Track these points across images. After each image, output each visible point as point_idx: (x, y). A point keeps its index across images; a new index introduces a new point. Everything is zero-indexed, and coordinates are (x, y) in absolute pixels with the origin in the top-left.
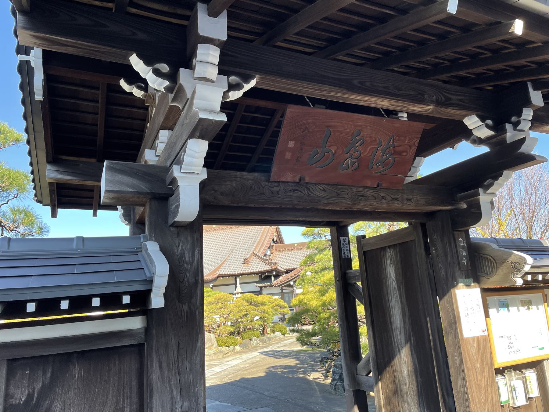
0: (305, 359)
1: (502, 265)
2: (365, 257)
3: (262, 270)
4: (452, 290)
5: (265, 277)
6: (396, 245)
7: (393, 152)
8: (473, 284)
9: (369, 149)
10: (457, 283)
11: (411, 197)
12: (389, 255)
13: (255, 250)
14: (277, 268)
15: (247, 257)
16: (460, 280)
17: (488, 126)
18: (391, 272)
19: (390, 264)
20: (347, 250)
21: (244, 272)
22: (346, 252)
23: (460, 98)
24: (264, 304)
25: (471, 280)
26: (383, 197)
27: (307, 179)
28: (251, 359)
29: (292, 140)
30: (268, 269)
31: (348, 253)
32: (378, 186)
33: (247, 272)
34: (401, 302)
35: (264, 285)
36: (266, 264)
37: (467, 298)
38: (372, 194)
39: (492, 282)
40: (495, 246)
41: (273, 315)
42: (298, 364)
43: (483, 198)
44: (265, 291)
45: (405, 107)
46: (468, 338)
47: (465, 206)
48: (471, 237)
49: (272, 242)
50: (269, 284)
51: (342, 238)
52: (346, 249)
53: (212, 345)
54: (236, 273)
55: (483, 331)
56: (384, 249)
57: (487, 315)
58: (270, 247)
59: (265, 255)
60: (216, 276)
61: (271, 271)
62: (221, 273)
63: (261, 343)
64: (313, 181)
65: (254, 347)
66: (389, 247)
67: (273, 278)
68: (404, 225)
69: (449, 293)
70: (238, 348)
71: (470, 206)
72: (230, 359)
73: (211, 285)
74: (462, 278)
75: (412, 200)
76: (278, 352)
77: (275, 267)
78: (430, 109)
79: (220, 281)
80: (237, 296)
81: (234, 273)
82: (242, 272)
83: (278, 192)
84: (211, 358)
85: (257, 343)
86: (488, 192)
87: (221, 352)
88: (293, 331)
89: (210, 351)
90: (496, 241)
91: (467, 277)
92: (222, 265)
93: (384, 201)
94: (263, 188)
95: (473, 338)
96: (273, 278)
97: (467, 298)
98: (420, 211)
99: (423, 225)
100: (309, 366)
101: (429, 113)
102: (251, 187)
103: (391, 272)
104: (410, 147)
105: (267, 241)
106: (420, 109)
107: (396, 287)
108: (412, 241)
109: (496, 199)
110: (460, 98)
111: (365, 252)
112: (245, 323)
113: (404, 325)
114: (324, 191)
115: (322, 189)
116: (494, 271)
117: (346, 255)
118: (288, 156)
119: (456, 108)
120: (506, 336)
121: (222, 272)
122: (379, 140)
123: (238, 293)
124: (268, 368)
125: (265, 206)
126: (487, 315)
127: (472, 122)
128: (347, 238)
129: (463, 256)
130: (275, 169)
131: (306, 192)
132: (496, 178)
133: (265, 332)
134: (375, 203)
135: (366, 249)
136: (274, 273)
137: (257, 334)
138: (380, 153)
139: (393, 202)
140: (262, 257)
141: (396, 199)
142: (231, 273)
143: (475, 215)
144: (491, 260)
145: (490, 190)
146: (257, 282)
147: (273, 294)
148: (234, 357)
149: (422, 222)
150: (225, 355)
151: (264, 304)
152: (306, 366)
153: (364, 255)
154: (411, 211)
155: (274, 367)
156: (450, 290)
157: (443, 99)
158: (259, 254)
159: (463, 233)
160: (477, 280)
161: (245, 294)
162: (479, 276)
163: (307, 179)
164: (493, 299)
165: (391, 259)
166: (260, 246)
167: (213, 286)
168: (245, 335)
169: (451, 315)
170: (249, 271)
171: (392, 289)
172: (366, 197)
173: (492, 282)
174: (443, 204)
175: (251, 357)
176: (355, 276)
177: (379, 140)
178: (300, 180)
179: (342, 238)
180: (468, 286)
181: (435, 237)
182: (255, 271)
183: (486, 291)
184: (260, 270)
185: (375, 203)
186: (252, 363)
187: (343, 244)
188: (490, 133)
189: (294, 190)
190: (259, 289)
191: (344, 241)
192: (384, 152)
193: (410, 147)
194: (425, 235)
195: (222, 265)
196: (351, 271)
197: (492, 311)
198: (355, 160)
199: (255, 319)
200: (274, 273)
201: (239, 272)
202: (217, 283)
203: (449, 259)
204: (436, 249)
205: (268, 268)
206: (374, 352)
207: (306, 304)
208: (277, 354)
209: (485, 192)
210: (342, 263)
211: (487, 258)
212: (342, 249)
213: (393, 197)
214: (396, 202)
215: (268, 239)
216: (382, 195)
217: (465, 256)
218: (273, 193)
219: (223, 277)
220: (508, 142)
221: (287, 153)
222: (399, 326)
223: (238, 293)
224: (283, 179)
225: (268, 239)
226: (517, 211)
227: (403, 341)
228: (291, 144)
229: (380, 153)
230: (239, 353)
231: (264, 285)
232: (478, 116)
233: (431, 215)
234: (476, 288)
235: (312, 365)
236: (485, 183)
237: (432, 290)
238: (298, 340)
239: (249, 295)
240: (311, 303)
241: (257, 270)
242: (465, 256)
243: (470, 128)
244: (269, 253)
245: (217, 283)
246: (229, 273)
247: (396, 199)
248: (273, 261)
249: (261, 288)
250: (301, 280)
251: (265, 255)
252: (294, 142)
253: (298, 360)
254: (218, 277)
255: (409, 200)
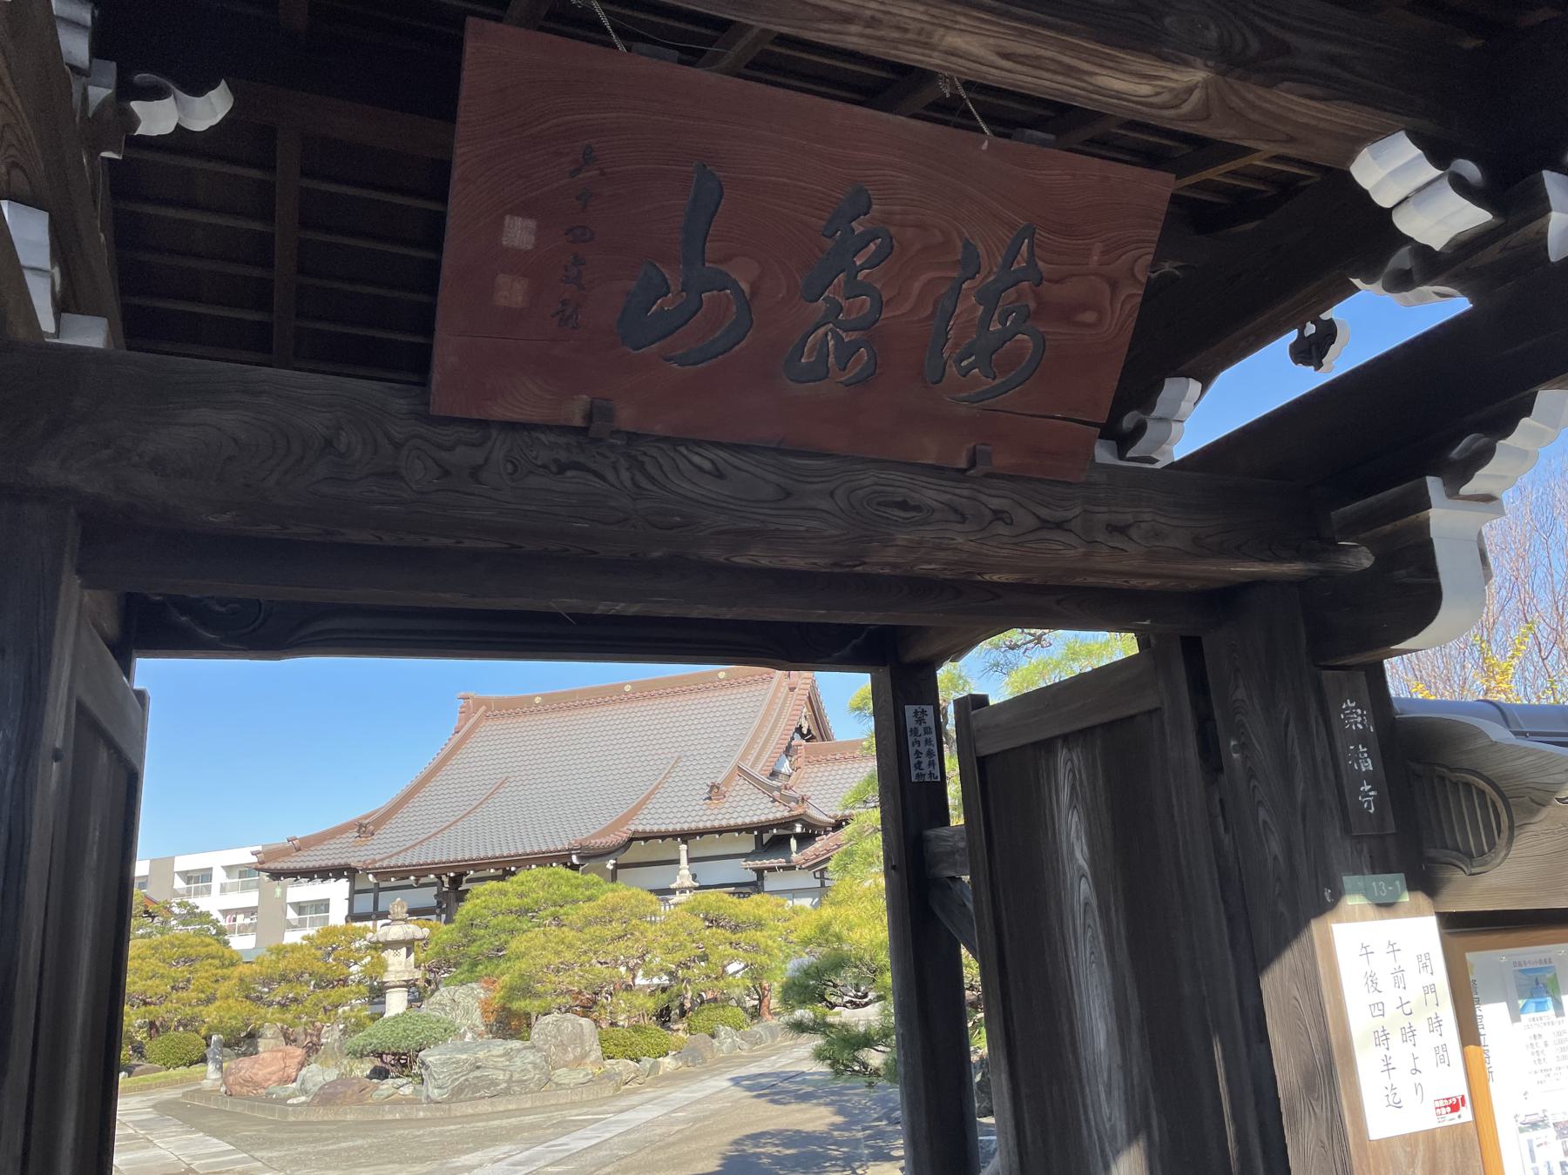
0: (862, 1111)
1: (1533, 813)
2: (984, 783)
3: (763, 818)
4: (1315, 926)
5: (772, 839)
6: (1091, 729)
7: (1032, 305)
8: (1406, 898)
9: (917, 286)
10: (1338, 895)
11: (1130, 518)
12: (1067, 777)
13: (743, 757)
14: (805, 814)
15: (719, 781)
16: (1348, 881)
17: (1461, 186)
18: (1074, 842)
19: (1072, 806)
20: (930, 753)
21: (709, 825)
22: (925, 760)
23: (1334, 49)
24: (759, 925)
25: (1398, 880)
26: (998, 515)
27: (626, 417)
28: (698, 1101)
29: (523, 210)
30: (779, 815)
31: (931, 764)
32: (973, 463)
33: (716, 824)
34: (1113, 964)
35: (766, 863)
36: (774, 801)
37: (1377, 960)
38: (945, 497)
39: (1482, 890)
40: (1498, 733)
41: (788, 956)
42: (836, 1127)
43: (1445, 518)
44: (771, 882)
45: (1070, 71)
46: (1388, 1141)
47: (1366, 560)
48: (1392, 693)
49: (797, 736)
50: (782, 861)
51: (910, 710)
52: (924, 749)
53: (585, 1055)
54: (686, 827)
55: (1455, 1108)
56: (1046, 746)
57: (1469, 1033)
58: (788, 751)
59: (774, 774)
60: (625, 837)
61: (787, 824)
62: (640, 828)
63: (746, 1046)
64: (659, 429)
65: (723, 1060)
66: (1066, 738)
67: (793, 842)
68: (1117, 646)
69: (1304, 938)
70: (668, 1063)
71: (1386, 560)
72: (635, 1099)
73: (610, 865)
74: (1356, 871)
75: (1134, 533)
76: (789, 1078)
77: (800, 811)
78: (1190, 90)
79: (638, 852)
80: (677, 898)
81: (678, 827)
82: (701, 825)
83: (475, 472)
84: (577, 1098)
85: (734, 1046)
86: (1466, 489)
87: (609, 1076)
88: (799, 1027)
89: (574, 1074)
90: (1502, 713)
91: (1381, 866)
92: (648, 797)
93: (1001, 529)
94: (398, 446)
95: (1410, 1140)
96: (793, 842)
97: (1377, 960)
98: (1171, 584)
99: (1192, 648)
100: (869, 1137)
101: (1191, 117)
102: (329, 443)
103: (1074, 842)
104: (1114, 285)
105: (782, 733)
106: (1144, 89)
107: (1094, 903)
108: (1150, 712)
109: (1494, 531)
110: (1334, 49)
111: (982, 762)
112: (697, 981)
113: (1124, 1058)
114: (719, 474)
115: (707, 465)
116: (1501, 842)
117: (926, 771)
118: (512, 292)
119: (1317, 92)
120: (1551, 1121)
121: (642, 824)
122: (967, 245)
123: (683, 891)
124: (736, 1142)
125: (434, 541)
126: (1469, 1033)
127: (1390, 170)
128: (930, 709)
129: (1360, 777)
130: (447, 351)
131: (625, 475)
132: (1504, 425)
133: (764, 1009)
134: (961, 540)
135: (987, 748)
136: (798, 829)
137: (735, 1016)
138: (969, 306)
139: (1045, 534)
140: (764, 779)
141: (1059, 526)
142: (670, 828)
143: (1409, 595)
144: (1482, 793)
145: (1478, 483)
146: (746, 856)
147: (795, 893)
148: (650, 1093)
149: (1188, 630)
150: (621, 1086)
151: (759, 925)
152: (860, 1135)
153: (979, 770)
154: (1134, 582)
155: (756, 1138)
156: (1307, 923)
157: (1255, 45)
158: (755, 772)
159: (1361, 679)
160: (1425, 881)
161: (701, 894)
162: (1433, 860)
163: (626, 417)
164: (1493, 959)
165: (1073, 788)
166: (757, 748)
167: (617, 866)
168: (699, 1021)
169: (1313, 1033)
170: (724, 823)
171: (1079, 909)
172: (917, 508)
173: (1482, 890)
174: (1273, 549)
175: (699, 1095)
176: (952, 853)
177: (967, 245)
178: (589, 416)
179: (910, 710)
180: (1386, 906)
181: (1240, 694)
182: (740, 821)
183: (1452, 924)
184: (755, 819)
185: (961, 540)
186: (696, 1120)
187: (915, 732)
188: (1473, 216)
189: (562, 468)
190: (753, 877)
191: (920, 721)
192: (989, 298)
193: (1114, 285)
194: (1199, 686)
195: (648, 797)
196: (943, 831)
197: (1492, 1015)
198: (854, 335)
199: (731, 969)
200: (798, 829)
201: (693, 826)
202: (626, 857)
203: (1300, 787)
204: (1243, 747)
205: (779, 812)
206: (1015, 1159)
207: (839, 938)
208: (786, 1084)
209: (1452, 492)
210: (909, 800)
211: (1468, 785)
212: (912, 750)
213: (1044, 512)
214: (1058, 535)
215: (782, 724)
216: (995, 503)
217: (1370, 777)
218: (446, 473)
219: (646, 839)
220: (1553, 259)
221: (502, 279)
222: (1105, 1065)
223: (683, 891)
224: (499, 411)
225: (782, 724)
226: (1544, 633)
227: (1121, 1126)
228: (519, 233)
229: (969, 306)
230: (673, 1078)
231: (766, 863)
232: (1418, 139)
233: (1224, 600)
234: (1418, 913)
235: (880, 1134)
236: (1455, 454)
237: (1230, 919)
238: (819, 1055)
239: (712, 895)
240: (855, 936)
241: (748, 820)
242: (1370, 777)
243: (1384, 200)
244: (786, 768)
245: (626, 857)
246: (663, 828)
247: (1059, 526)
248: (798, 792)
249: (760, 872)
250: (846, 853)
251: (774, 774)
252: (532, 224)
253: (839, 1113)
254: (631, 840)
255: (1121, 530)
